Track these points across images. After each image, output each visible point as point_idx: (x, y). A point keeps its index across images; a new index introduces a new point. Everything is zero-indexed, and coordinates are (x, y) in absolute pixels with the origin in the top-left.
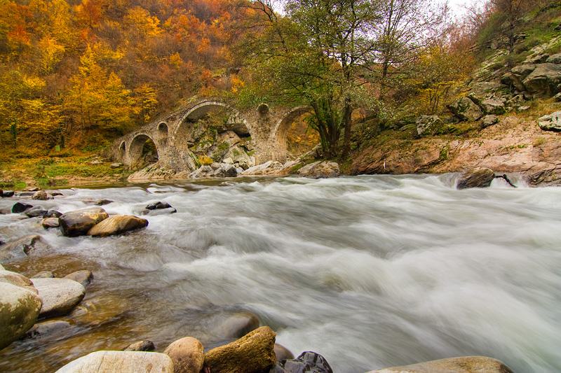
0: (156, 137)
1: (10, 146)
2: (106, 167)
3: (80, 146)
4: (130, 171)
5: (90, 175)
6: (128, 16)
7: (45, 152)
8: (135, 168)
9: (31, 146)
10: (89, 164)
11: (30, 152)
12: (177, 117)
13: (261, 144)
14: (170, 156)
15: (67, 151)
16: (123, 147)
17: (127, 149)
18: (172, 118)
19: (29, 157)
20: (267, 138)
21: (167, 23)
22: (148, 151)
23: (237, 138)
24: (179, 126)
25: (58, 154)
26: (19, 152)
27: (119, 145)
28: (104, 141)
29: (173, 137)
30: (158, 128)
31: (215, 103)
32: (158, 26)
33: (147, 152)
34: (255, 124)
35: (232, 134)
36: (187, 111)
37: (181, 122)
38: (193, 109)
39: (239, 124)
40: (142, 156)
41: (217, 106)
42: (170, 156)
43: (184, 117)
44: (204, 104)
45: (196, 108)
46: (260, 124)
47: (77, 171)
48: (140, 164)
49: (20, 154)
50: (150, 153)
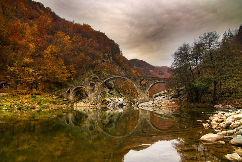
0: (88, 89)
1: (13, 88)
2: (61, 100)
3: (44, 90)
4: (71, 102)
5: (56, 104)
6: (57, 34)
7: (29, 92)
8: (73, 101)
9: (23, 89)
10: (53, 98)
11: (23, 92)
12: (101, 81)
13: (141, 94)
14: (95, 97)
15: (38, 92)
16: (69, 92)
17: (71, 92)
18: (98, 81)
19: (23, 94)
20: (145, 92)
21: (73, 39)
22: (177, 116)
23: (108, 90)
24: (101, 84)
25: (35, 93)
26: (18, 92)
27: (66, 91)
28: (55, 88)
29: (98, 89)
30: (89, 85)
31: (120, 77)
32: (69, 39)
33: (78, 94)
34: (139, 86)
35: (107, 88)
36: (106, 79)
37: (102, 83)
38: (109, 78)
39: (110, 84)
40: (76, 96)
41: (121, 78)
42: (95, 97)
43: (104, 81)
44: (115, 77)
45: (110, 78)
46: (141, 87)
47: (51, 102)
48: (75, 100)
49: (19, 93)
50: (79, 95)
